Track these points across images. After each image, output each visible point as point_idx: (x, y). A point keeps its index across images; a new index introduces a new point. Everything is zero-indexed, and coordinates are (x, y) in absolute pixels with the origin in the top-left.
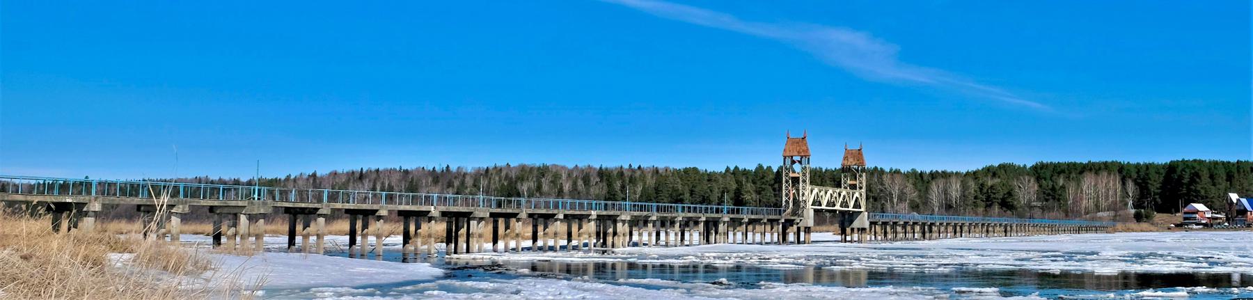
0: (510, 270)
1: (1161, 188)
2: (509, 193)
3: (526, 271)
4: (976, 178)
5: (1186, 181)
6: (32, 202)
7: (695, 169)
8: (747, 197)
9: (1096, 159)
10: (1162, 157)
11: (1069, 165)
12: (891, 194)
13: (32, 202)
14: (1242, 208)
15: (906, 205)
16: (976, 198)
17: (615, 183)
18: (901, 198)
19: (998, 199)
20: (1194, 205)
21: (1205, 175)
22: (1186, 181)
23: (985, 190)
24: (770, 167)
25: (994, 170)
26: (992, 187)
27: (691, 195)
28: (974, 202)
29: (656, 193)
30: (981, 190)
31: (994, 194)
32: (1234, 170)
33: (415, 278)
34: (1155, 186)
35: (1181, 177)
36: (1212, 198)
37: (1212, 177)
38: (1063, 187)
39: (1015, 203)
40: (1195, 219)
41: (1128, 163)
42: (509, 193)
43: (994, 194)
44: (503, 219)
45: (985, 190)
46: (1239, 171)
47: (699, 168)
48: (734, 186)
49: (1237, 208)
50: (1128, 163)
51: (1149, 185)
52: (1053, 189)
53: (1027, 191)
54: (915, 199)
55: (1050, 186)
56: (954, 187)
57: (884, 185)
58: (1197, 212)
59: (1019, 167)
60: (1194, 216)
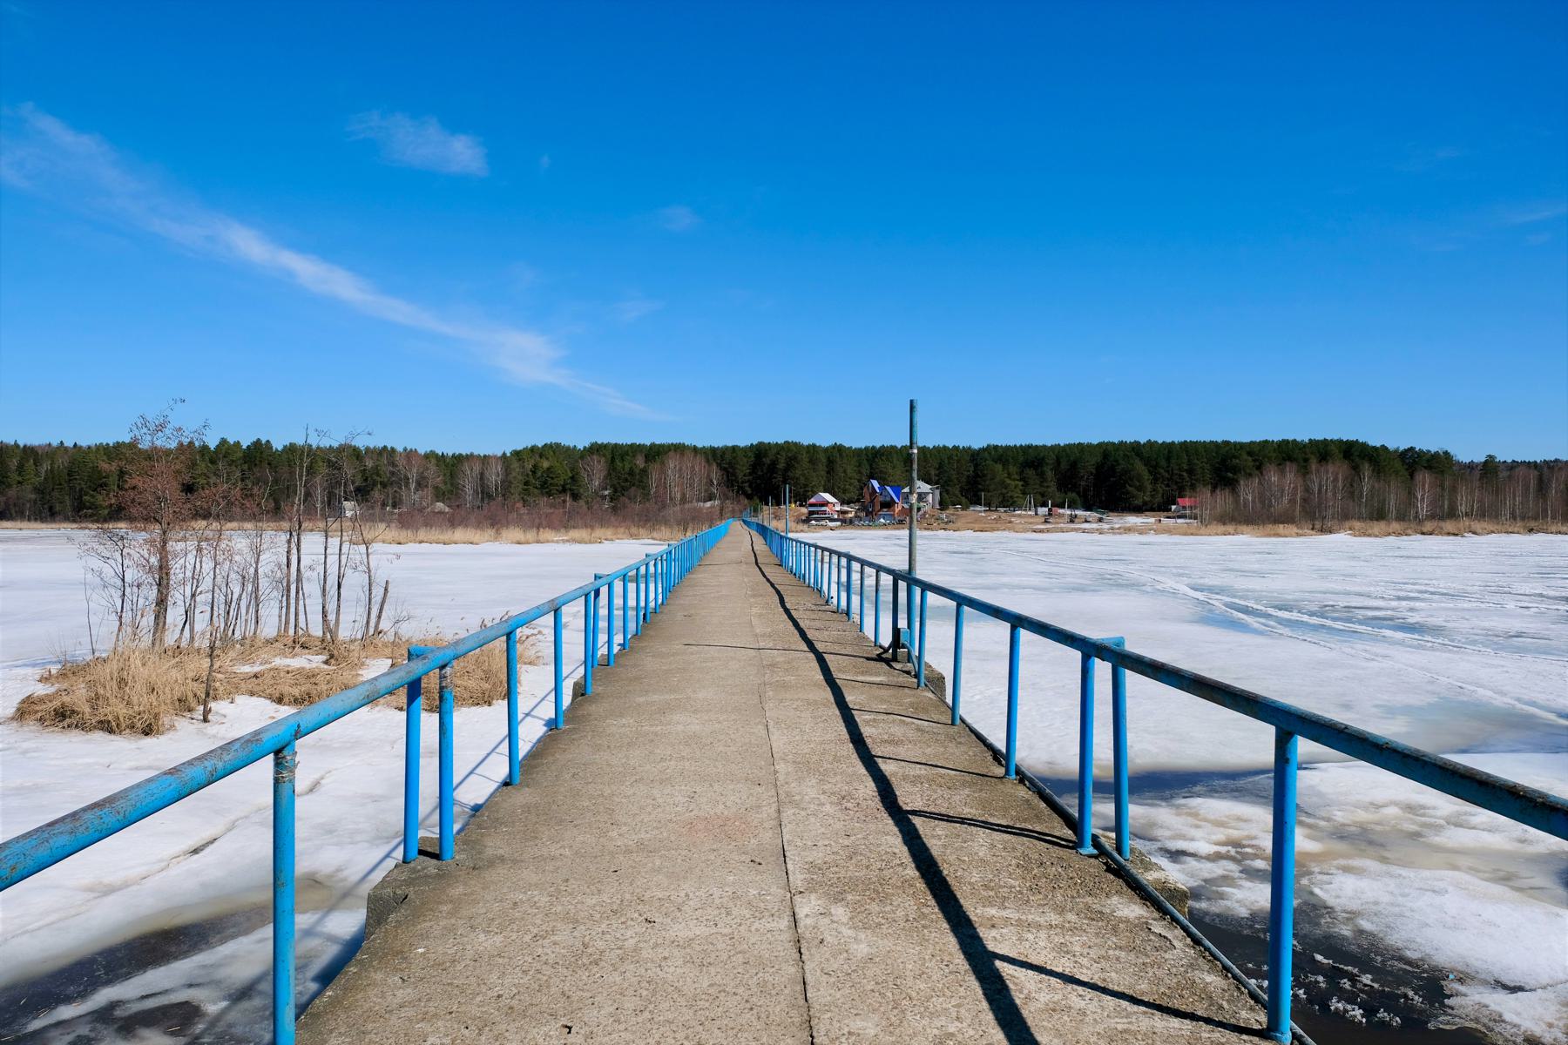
0: (111, 673)
1: (750, 474)
3: (1027, 782)
4: (520, 460)
5: (781, 466)
6: (1294, 946)
9: (1303, 432)
10: (742, 435)
11: (632, 446)
13: (1294, 946)
14: (888, 499)
15: (429, 492)
16: (526, 483)
17: (11, 461)
18: (420, 485)
19: (557, 485)
20: (823, 494)
21: (805, 457)
22: (781, 466)
23: (539, 474)
24: (238, 442)
25: (541, 451)
26: (548, 469)
28: (525, 490)
29: (68, 474)
30: (534, 472)
31: (552, 478)
32: (836, 454)
34: (743, 470)
35: (774, 463)
36: (812, 487)
38: (644, 471)
39: (581, 490)
40: (825, 511)
43: (552, 478)
46: (841, 455)
49: (881, 499)
51: (737, 471)
52: (631, 473)
53: (596, 474)
54: (440, 485)
55: (627, 469)
56: (494, 470)
57: (397, 466)
58: (826, 504)
59: (568, 448)
60: (823, 509)
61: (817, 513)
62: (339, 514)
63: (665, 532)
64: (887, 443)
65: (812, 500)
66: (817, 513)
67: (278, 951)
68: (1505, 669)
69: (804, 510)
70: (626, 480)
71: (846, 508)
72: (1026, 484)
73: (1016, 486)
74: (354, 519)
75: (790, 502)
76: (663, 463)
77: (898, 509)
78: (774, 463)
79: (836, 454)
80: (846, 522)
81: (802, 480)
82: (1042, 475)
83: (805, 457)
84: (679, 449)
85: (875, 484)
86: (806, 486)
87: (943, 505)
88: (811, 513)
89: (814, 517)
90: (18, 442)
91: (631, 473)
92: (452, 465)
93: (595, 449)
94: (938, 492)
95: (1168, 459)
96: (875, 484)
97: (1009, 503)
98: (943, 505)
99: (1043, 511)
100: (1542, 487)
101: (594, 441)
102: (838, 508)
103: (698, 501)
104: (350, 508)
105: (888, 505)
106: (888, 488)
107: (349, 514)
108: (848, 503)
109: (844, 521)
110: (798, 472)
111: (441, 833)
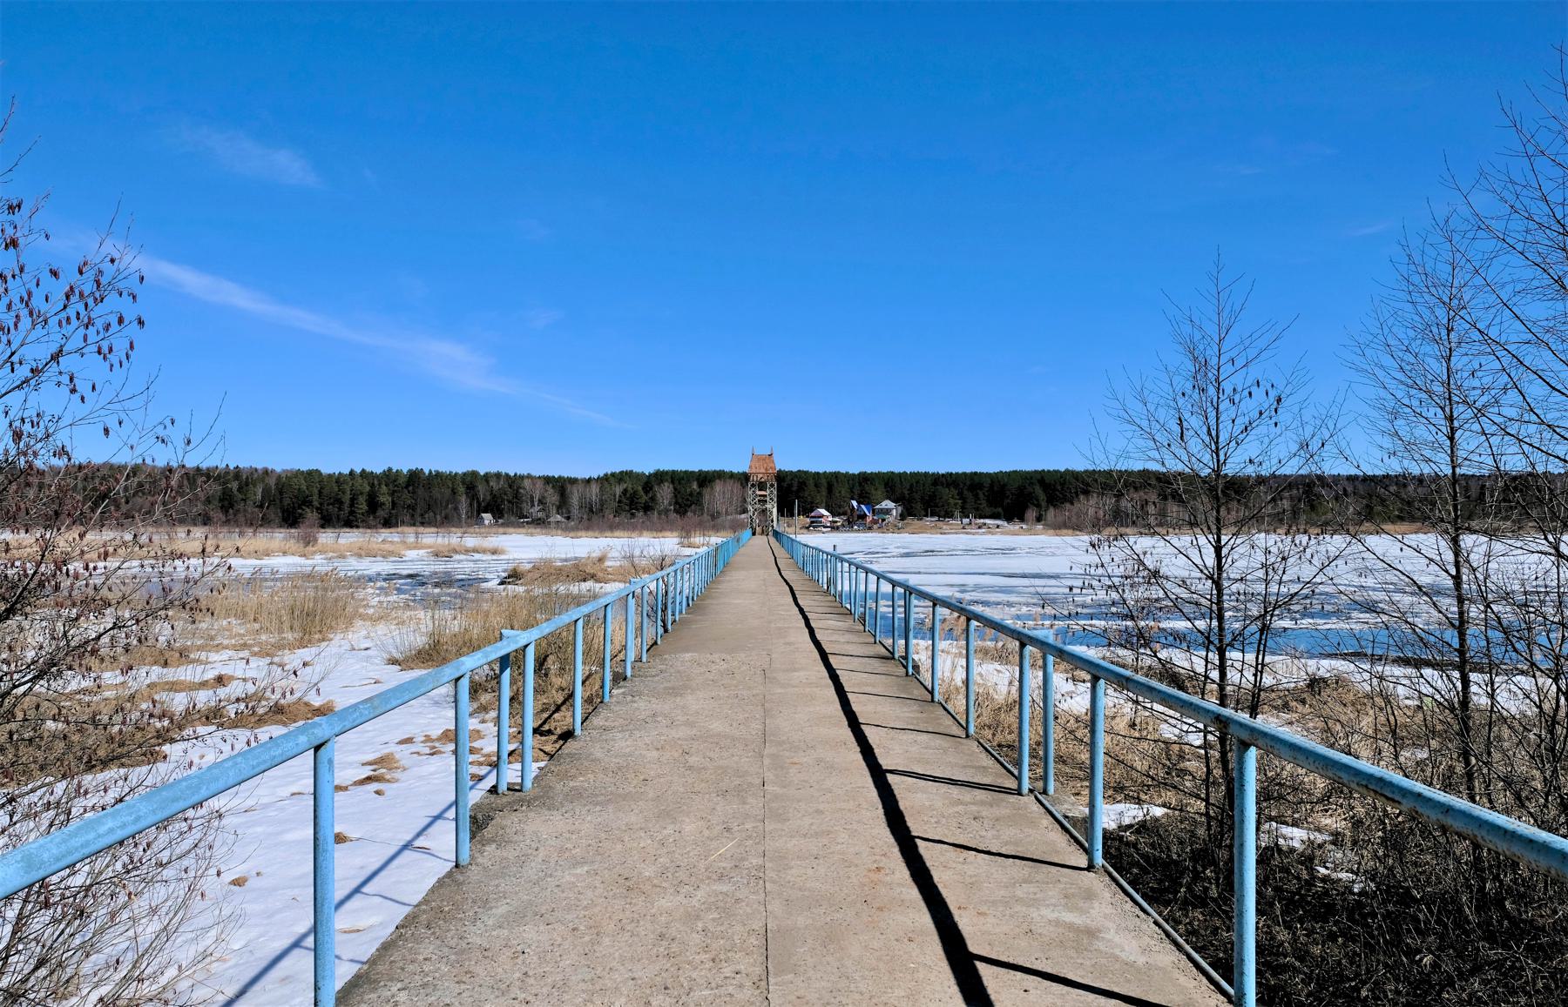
2: (25, 486)
5: (794, 489)
7: (317, 471)
8: (382, 499)
12: (532, 497)
21: (811, 482)
22: (794, 489)
23: (628, 495)
27: (320, 495)
32: (834, 480)
33: (278, 952)
35: (790, 486)
37: (816, 485)
38: (700, 494)
40: (821, 522)
41: (363, 470)
42: (25, 486)
44: (1227, 653)
45: (628, 495)
47: (323, 471)
48: (368, 488)
49: (858, 513)
50: (363, 470)
52: (691, 494)
53: (665, 493)
58: (822, 516)
61: (816, 522)
62: (480, 522)
63: (723, 533)
64: (876, 470)
65: (813, 514)
66: (816, 522)
67: (318, 865)
68: (1049, 610)
69: (808, 520)
70: (688, 500)
71: (837, 519)
72: (964, 502)
73: (956, 504)
74: (491, 525)
75: (799, 515)
76: (712, 488)
77: (869, 519)
78: (790, 486)
79: (834, 480)
80: (834, 528)
81: (809, 499)
82: (976, 497)
83: (811, 482)
84: (720, 475)
85: (855, 503)
86: (812, 503)
87: (903, 517)
88: (812, 522)
89: (814, 525)
90: (775, 457)
91: (691, 494)
92: (561, 486)
93: (660, 477)
94: (900, 509)
95: (1062, 484)
96: (855, 503)
97: (949, 515)
98: (903, 517)
99: (966, 521)
100: (373, 505)
101: (657, 468)
102: (831, 519)
103: (736, 513)
104: (487, 517)
105: (863, 517)
106: (863, 506)
107: (487, 522)
108: (839, 515)
109: (832, 528)
110: (806, 494)
111: (522, 771)
